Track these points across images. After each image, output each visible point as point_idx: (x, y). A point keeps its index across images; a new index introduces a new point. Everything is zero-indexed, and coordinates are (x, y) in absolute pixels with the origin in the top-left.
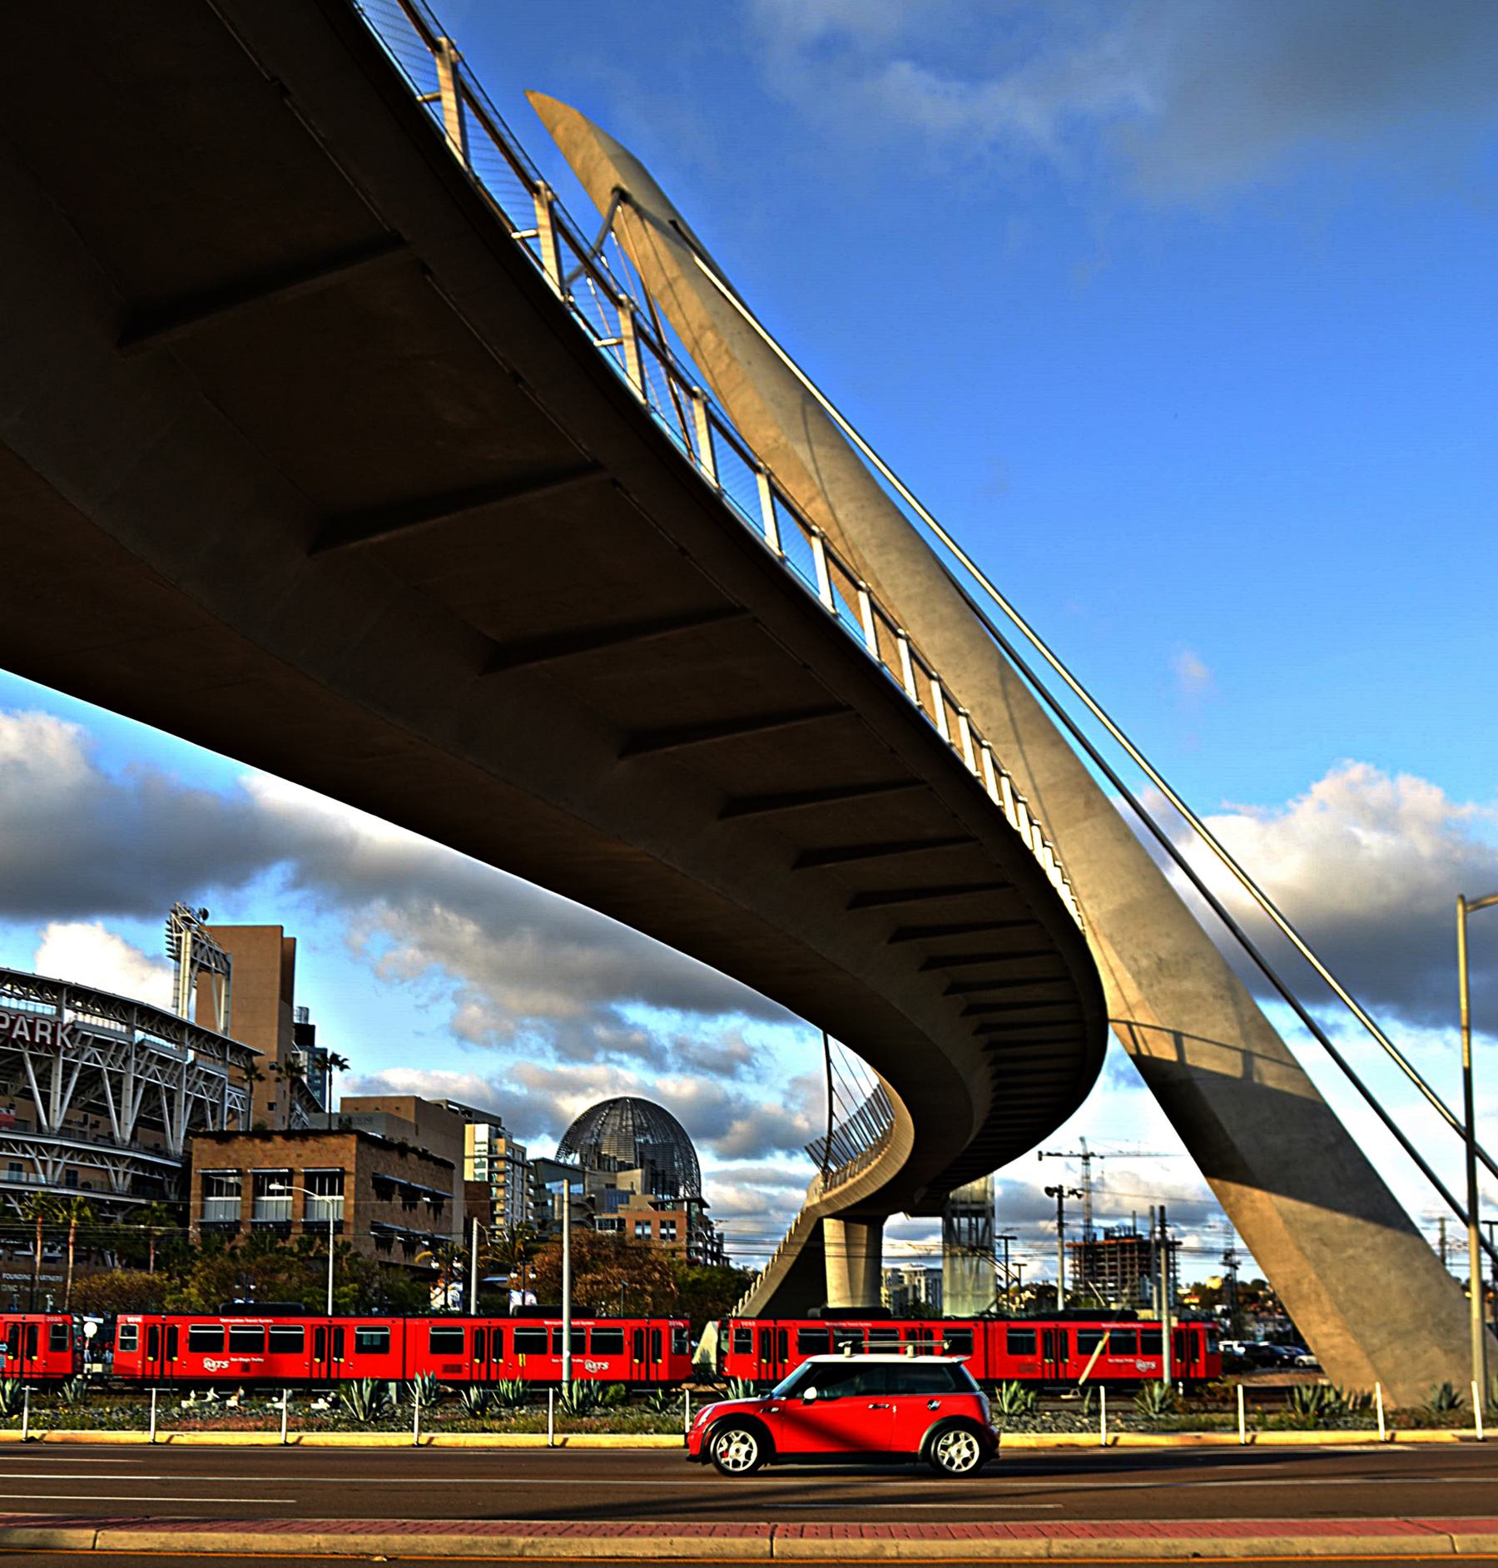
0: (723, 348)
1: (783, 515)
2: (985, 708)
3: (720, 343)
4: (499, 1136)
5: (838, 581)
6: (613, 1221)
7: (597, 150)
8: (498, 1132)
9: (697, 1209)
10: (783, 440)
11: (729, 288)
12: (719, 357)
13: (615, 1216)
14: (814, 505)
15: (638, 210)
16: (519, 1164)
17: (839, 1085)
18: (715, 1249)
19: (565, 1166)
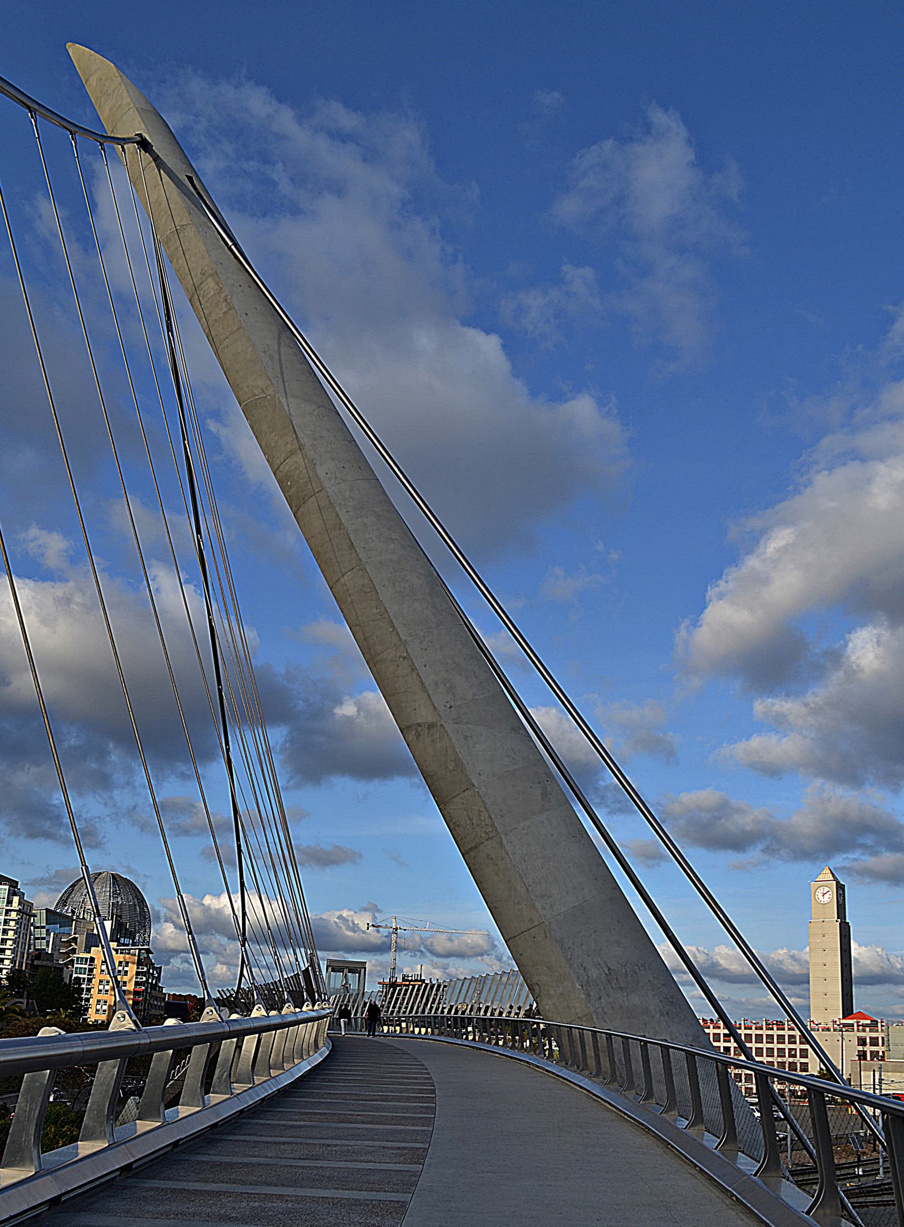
0: (223, 295)
1: (165, 178)
2: (448, 685)
3: (220, 291)
4: (15, 894)
5: (167, 183)
6: (86, 959)
7: (127, 100)
8: (14, 891)
9: (146, 955)
10: (270, 391)
11: (236, 245)
12: (217, 304)
13: (88, 956)
14: (294, 458)
15: (156, 158)
16: (27, 914)
17: (243, 811)
18: (154, 982)
19: (61, 915)
